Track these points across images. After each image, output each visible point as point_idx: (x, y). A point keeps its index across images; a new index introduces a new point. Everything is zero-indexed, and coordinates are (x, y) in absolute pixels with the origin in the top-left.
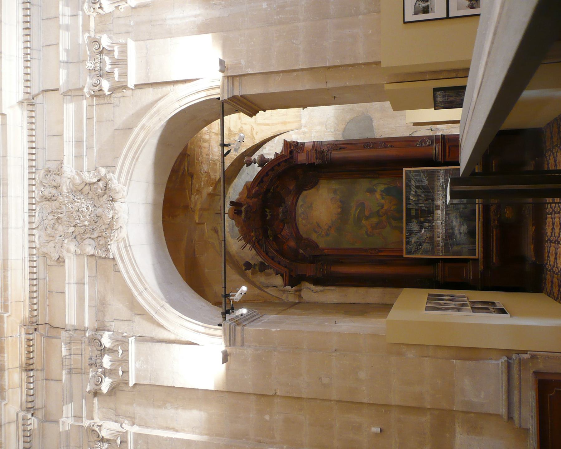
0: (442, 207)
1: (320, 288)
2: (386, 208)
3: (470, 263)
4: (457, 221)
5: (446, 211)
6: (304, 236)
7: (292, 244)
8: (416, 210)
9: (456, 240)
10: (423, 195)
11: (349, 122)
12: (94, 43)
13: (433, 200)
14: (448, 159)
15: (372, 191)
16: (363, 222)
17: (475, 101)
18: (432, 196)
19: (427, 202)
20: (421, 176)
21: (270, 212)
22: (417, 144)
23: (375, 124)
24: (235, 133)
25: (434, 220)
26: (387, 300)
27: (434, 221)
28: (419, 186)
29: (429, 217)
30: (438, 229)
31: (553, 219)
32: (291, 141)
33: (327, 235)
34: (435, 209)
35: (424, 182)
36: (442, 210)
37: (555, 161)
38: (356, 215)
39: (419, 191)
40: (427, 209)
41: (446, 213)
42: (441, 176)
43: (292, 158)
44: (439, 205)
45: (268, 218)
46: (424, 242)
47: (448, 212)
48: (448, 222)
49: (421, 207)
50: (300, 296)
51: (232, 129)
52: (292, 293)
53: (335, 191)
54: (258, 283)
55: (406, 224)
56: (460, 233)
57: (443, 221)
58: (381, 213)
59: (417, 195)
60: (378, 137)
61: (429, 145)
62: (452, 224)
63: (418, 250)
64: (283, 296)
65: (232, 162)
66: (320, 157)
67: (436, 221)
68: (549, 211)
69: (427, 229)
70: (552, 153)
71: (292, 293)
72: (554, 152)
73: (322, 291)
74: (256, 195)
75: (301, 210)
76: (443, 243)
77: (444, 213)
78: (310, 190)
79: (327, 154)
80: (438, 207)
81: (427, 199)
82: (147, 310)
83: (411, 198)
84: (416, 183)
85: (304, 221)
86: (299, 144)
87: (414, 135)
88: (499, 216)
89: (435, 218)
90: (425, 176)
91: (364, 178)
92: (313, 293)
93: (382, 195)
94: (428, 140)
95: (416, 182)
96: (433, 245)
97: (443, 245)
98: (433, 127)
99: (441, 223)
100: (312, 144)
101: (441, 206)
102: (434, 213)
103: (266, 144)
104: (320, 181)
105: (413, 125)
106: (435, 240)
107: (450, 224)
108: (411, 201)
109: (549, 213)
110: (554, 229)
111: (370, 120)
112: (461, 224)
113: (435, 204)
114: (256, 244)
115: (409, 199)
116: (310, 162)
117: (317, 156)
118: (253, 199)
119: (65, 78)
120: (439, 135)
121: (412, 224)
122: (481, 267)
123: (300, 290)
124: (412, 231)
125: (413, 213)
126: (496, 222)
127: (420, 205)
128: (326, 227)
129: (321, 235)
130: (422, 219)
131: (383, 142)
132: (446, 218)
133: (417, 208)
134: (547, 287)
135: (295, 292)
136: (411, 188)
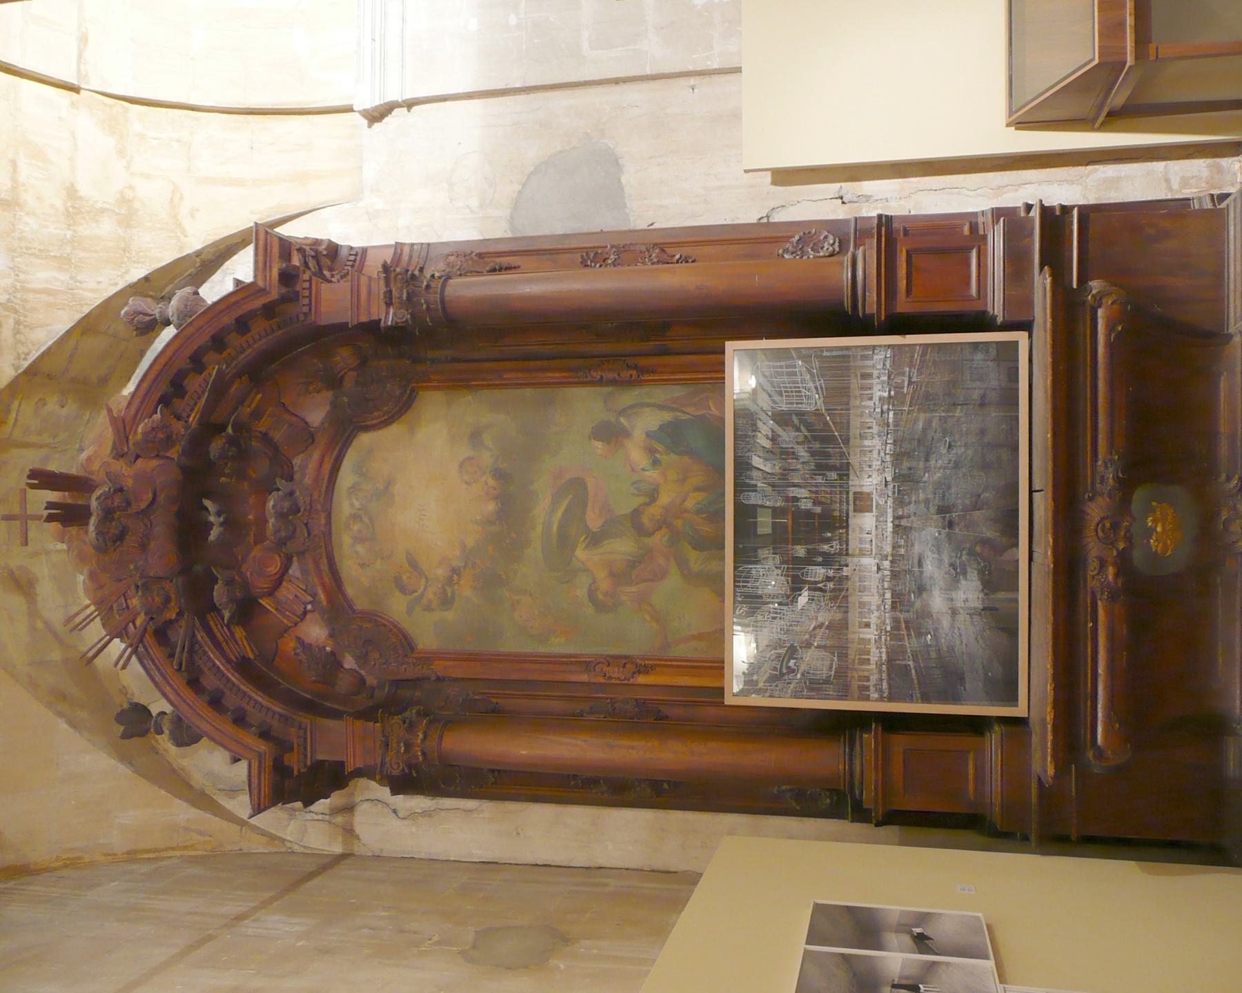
0: (882, 502)
1: (419, 803)
2: (664, 499)
3: (994, 738)
4: (941, 561)
5: (897, 518)
6: (361, 604)
7: (315, 632)
8: (776, 512)
9: (935, 637)
10: (802, 452)
11: (532, 173)
13: (844, 471)
14: (903, 305)
15: (611, 434)
16: (580, 553)
18: (842, 454)
19: (819, 479)
20: (794, 374)
21: (219, 514)
22: (786, 251)
23: (629, 178)
24: (99, 205)
25: (847, 554)
26: (672, 858)
27: (849, 559)
28: (790, 413)
29: (828, 541)
30: (863, 589)
32: (306, 238)
33: (446, 602)
34: (851, 508)
35: (808, 397)
36: (882, 513)
38: (555, 528)
39: (787, 436)
40: (818, 510)
41: (896, 527)
42: (875, 373)
43: (289, 298)
44: (869, 494)
45: (214, 534)
46: (808, 645)
47: (904, 522)
48: (903, 566)
49: (796, 499)
50: (349, 832)
51: (83, 190)
52: (320, 817)
53: (475, 437)
54: (198, 779)
55: (735, 568)
56: (954, 612)
57: (886, 557)
58: (645, 520)
59: (782, 453)
60: (641, 225)
61: (831, 255)
62: (921, 572)
63: (782, 674)
64: (290, 828)
65: (78, 316)
66: (400, 298)
67: (855, 560)
69: (820, 590)
71: (320, 817)
73: (426, 814)
74: (157, 444)
75: (352, 505)
76: (884, 650)
77: (890, 525)
78: (380, 432)
79: (428, 287)
80: (862, 502)
81: (822, 468)
83: (757, 461)
84: (774, 402)
85: (360, 549)
86: (344, 253)
87: (777, 218)
88: (1121, 546)
89: (853, 545)
90: (812, 375)
91: (585, 384)
92: (395, 823)
93: (651, 451)
94: (826, 237)
95: (777, 398)
96: (843, 656)
97: (884, 657)
98: (849, 188)
99: (875, 568)
100: (391, 251)
101: (875, 496)
102: (847, 527)
103: (235, 257)
104: (421, 393)
105: (774, 183)
106: (851, 636)
107: (910, 572)
108: (755, 474)
111: (612, 163)
112: (957, 572)
113: (852, 490)
114: (149, 640)
115: (750, 467)
116: (364, 319)
117: (391, 292)
118: (140, 461)
120: (870, 218)
121: (756, 569)
122: (1042, 762)
123: (349, 809)
124: (761, 597)
125: (765, 523)
126: (1111, 571)
127: (793, 492)
128: (441, 572)
129: (424, 601)
130: (800, 551)
131: (655, 245)
132: (895, 547)
133: (778, 504)
135: (330, 815)
136: (755, 425)
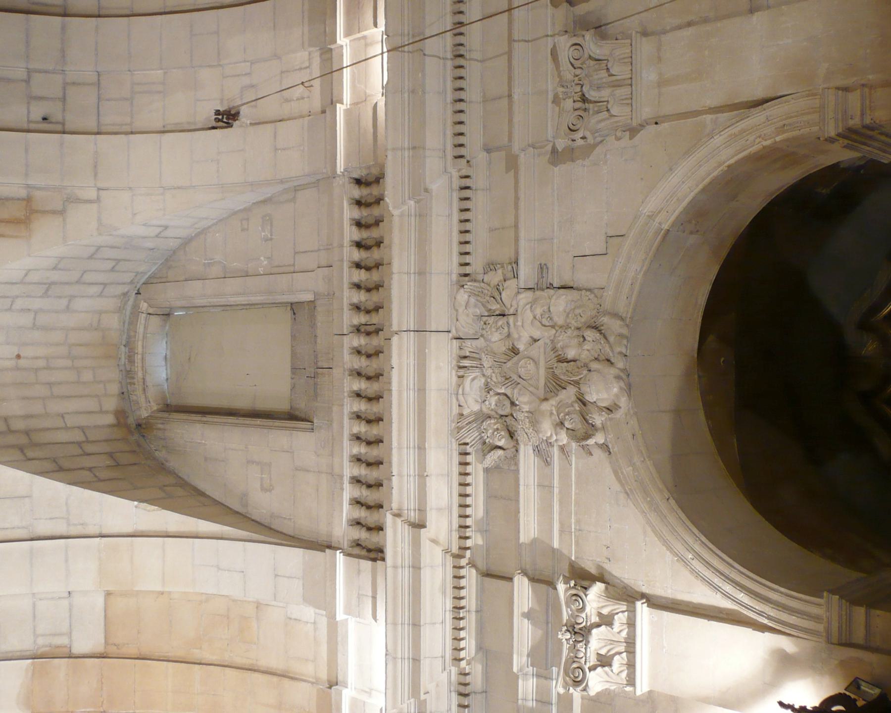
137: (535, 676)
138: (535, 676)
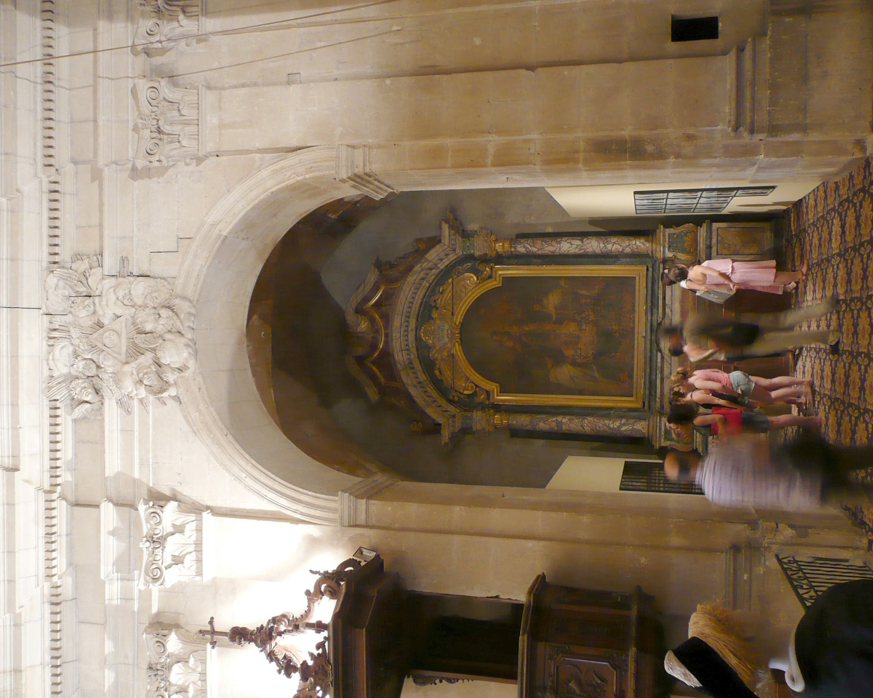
12: (153, 515)
17: (355, 24)
31: (833, 388)
37: (865, 270)
68: (856, 305)
70: (815, 229)
72: (818, 226)
82: (467, 308)
109: (856, 301)
110: (860, 379)
119: (113, 680)
134: (824, 412)
137: (119, 581)
138: (119, 581)
